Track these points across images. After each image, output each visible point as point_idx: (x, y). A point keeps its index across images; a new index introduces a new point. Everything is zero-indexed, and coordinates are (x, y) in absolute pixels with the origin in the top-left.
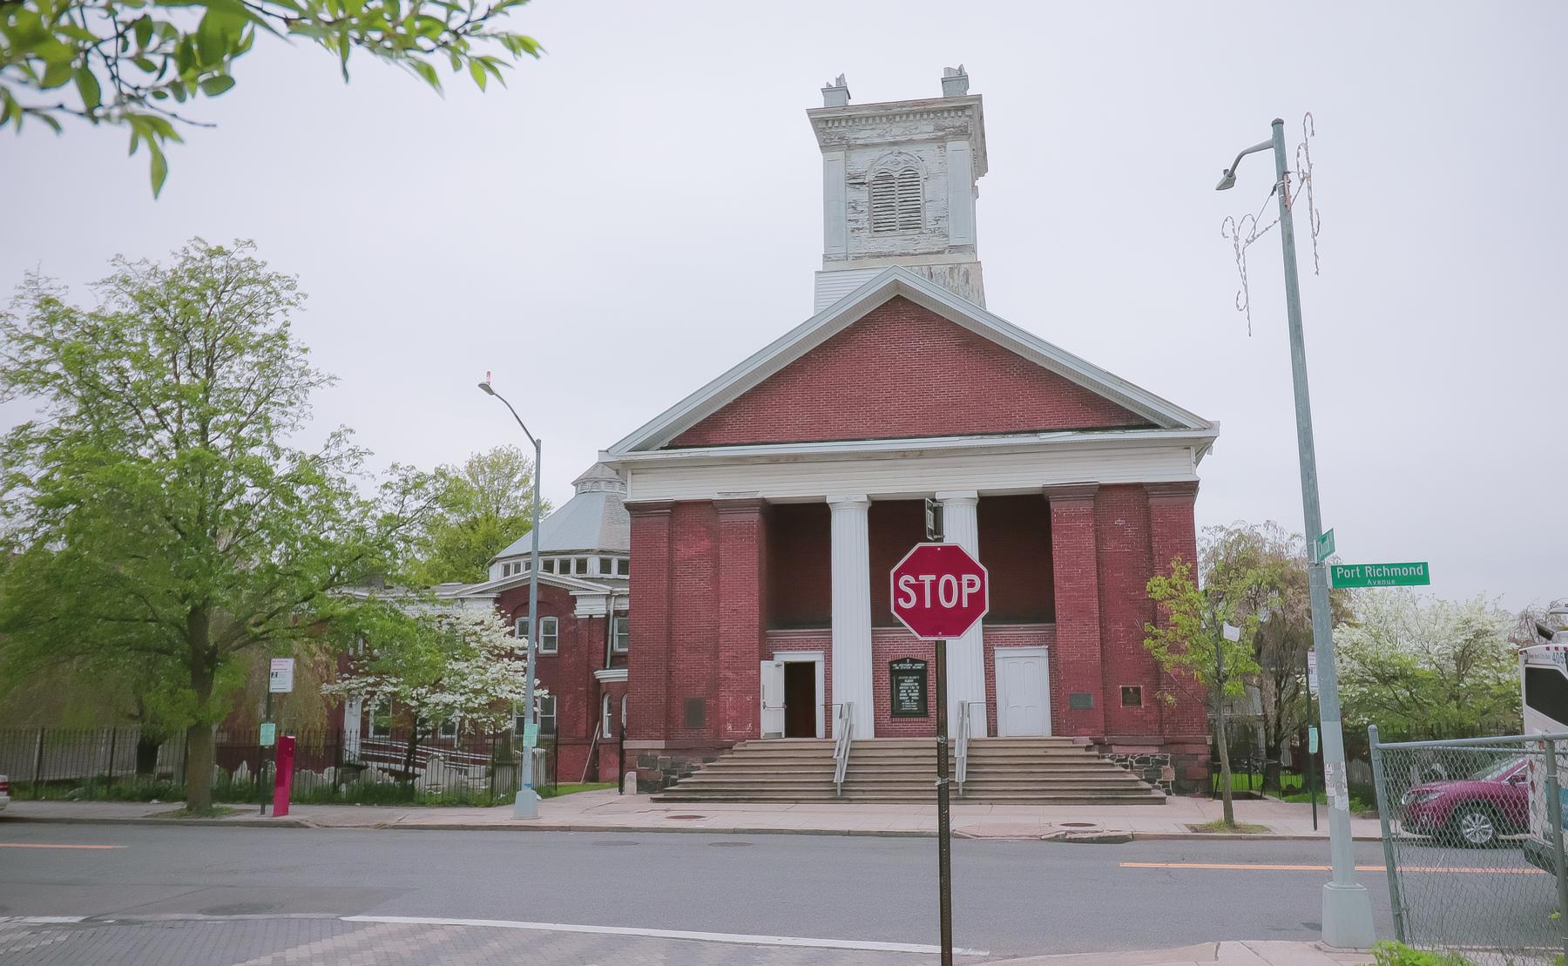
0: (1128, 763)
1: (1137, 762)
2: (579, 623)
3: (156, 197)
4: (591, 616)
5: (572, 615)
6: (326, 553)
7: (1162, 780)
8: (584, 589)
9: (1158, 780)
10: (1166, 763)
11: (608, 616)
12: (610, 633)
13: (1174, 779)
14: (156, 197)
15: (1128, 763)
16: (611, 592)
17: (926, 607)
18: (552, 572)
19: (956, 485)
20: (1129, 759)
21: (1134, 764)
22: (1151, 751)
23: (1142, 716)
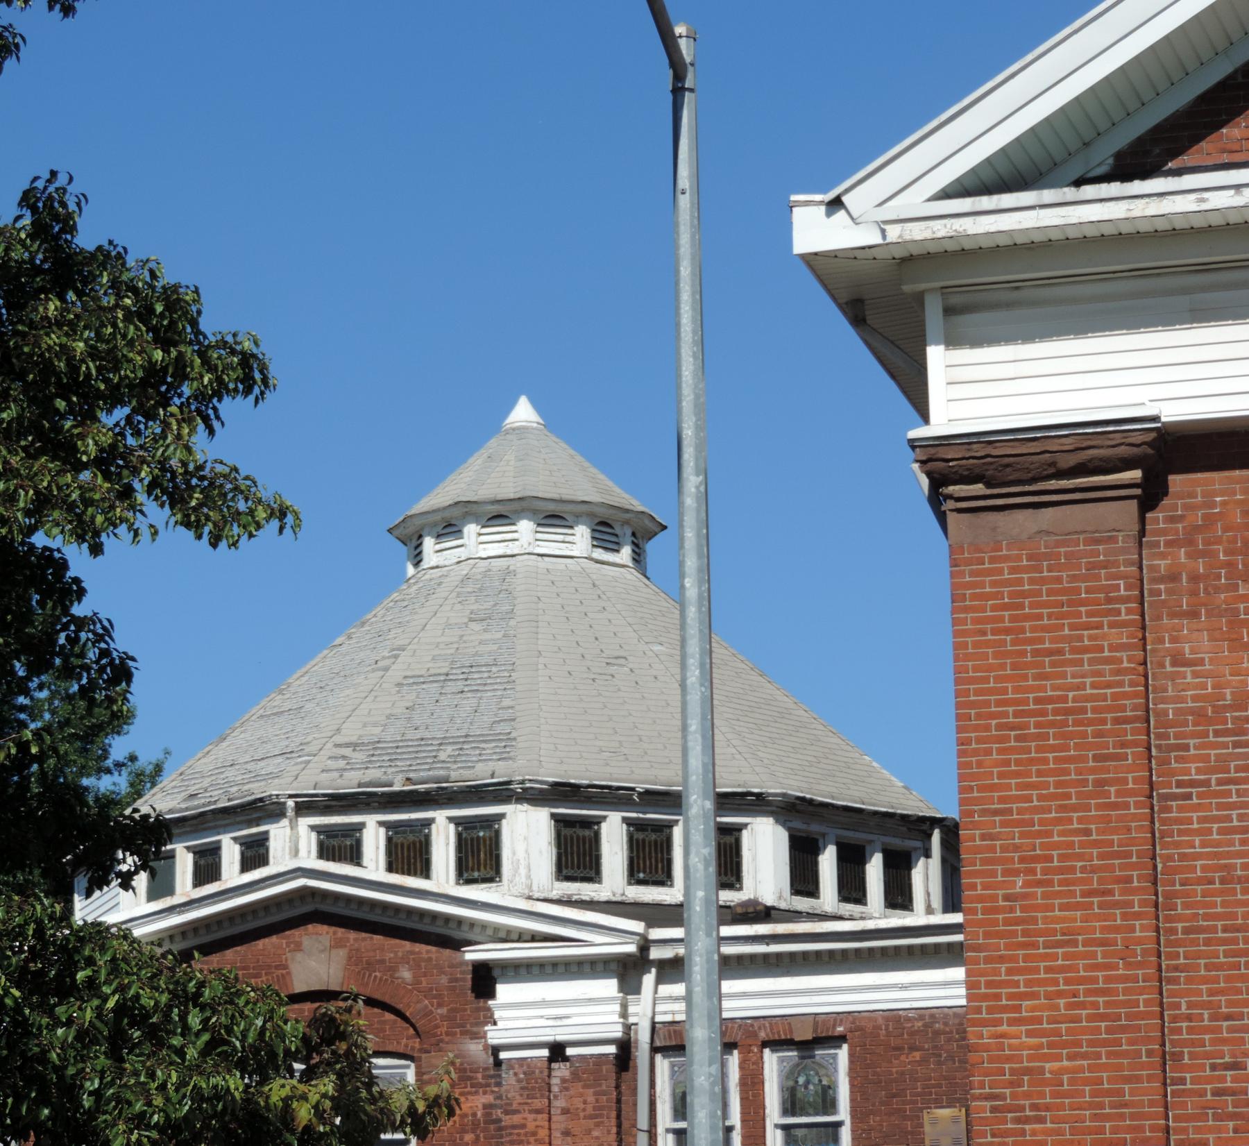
2: (508, 1078)
3: (929, 200)
4: (557, 1051)
5: (474, 1049)
6: (481, 834)
8: (535, 937)
11: (625, 1047)
12: (643, 1123)
14: (929, 200)
16: (645, 945)
17: (957, 997)
18: (424, 870)
19: (1010, 370)
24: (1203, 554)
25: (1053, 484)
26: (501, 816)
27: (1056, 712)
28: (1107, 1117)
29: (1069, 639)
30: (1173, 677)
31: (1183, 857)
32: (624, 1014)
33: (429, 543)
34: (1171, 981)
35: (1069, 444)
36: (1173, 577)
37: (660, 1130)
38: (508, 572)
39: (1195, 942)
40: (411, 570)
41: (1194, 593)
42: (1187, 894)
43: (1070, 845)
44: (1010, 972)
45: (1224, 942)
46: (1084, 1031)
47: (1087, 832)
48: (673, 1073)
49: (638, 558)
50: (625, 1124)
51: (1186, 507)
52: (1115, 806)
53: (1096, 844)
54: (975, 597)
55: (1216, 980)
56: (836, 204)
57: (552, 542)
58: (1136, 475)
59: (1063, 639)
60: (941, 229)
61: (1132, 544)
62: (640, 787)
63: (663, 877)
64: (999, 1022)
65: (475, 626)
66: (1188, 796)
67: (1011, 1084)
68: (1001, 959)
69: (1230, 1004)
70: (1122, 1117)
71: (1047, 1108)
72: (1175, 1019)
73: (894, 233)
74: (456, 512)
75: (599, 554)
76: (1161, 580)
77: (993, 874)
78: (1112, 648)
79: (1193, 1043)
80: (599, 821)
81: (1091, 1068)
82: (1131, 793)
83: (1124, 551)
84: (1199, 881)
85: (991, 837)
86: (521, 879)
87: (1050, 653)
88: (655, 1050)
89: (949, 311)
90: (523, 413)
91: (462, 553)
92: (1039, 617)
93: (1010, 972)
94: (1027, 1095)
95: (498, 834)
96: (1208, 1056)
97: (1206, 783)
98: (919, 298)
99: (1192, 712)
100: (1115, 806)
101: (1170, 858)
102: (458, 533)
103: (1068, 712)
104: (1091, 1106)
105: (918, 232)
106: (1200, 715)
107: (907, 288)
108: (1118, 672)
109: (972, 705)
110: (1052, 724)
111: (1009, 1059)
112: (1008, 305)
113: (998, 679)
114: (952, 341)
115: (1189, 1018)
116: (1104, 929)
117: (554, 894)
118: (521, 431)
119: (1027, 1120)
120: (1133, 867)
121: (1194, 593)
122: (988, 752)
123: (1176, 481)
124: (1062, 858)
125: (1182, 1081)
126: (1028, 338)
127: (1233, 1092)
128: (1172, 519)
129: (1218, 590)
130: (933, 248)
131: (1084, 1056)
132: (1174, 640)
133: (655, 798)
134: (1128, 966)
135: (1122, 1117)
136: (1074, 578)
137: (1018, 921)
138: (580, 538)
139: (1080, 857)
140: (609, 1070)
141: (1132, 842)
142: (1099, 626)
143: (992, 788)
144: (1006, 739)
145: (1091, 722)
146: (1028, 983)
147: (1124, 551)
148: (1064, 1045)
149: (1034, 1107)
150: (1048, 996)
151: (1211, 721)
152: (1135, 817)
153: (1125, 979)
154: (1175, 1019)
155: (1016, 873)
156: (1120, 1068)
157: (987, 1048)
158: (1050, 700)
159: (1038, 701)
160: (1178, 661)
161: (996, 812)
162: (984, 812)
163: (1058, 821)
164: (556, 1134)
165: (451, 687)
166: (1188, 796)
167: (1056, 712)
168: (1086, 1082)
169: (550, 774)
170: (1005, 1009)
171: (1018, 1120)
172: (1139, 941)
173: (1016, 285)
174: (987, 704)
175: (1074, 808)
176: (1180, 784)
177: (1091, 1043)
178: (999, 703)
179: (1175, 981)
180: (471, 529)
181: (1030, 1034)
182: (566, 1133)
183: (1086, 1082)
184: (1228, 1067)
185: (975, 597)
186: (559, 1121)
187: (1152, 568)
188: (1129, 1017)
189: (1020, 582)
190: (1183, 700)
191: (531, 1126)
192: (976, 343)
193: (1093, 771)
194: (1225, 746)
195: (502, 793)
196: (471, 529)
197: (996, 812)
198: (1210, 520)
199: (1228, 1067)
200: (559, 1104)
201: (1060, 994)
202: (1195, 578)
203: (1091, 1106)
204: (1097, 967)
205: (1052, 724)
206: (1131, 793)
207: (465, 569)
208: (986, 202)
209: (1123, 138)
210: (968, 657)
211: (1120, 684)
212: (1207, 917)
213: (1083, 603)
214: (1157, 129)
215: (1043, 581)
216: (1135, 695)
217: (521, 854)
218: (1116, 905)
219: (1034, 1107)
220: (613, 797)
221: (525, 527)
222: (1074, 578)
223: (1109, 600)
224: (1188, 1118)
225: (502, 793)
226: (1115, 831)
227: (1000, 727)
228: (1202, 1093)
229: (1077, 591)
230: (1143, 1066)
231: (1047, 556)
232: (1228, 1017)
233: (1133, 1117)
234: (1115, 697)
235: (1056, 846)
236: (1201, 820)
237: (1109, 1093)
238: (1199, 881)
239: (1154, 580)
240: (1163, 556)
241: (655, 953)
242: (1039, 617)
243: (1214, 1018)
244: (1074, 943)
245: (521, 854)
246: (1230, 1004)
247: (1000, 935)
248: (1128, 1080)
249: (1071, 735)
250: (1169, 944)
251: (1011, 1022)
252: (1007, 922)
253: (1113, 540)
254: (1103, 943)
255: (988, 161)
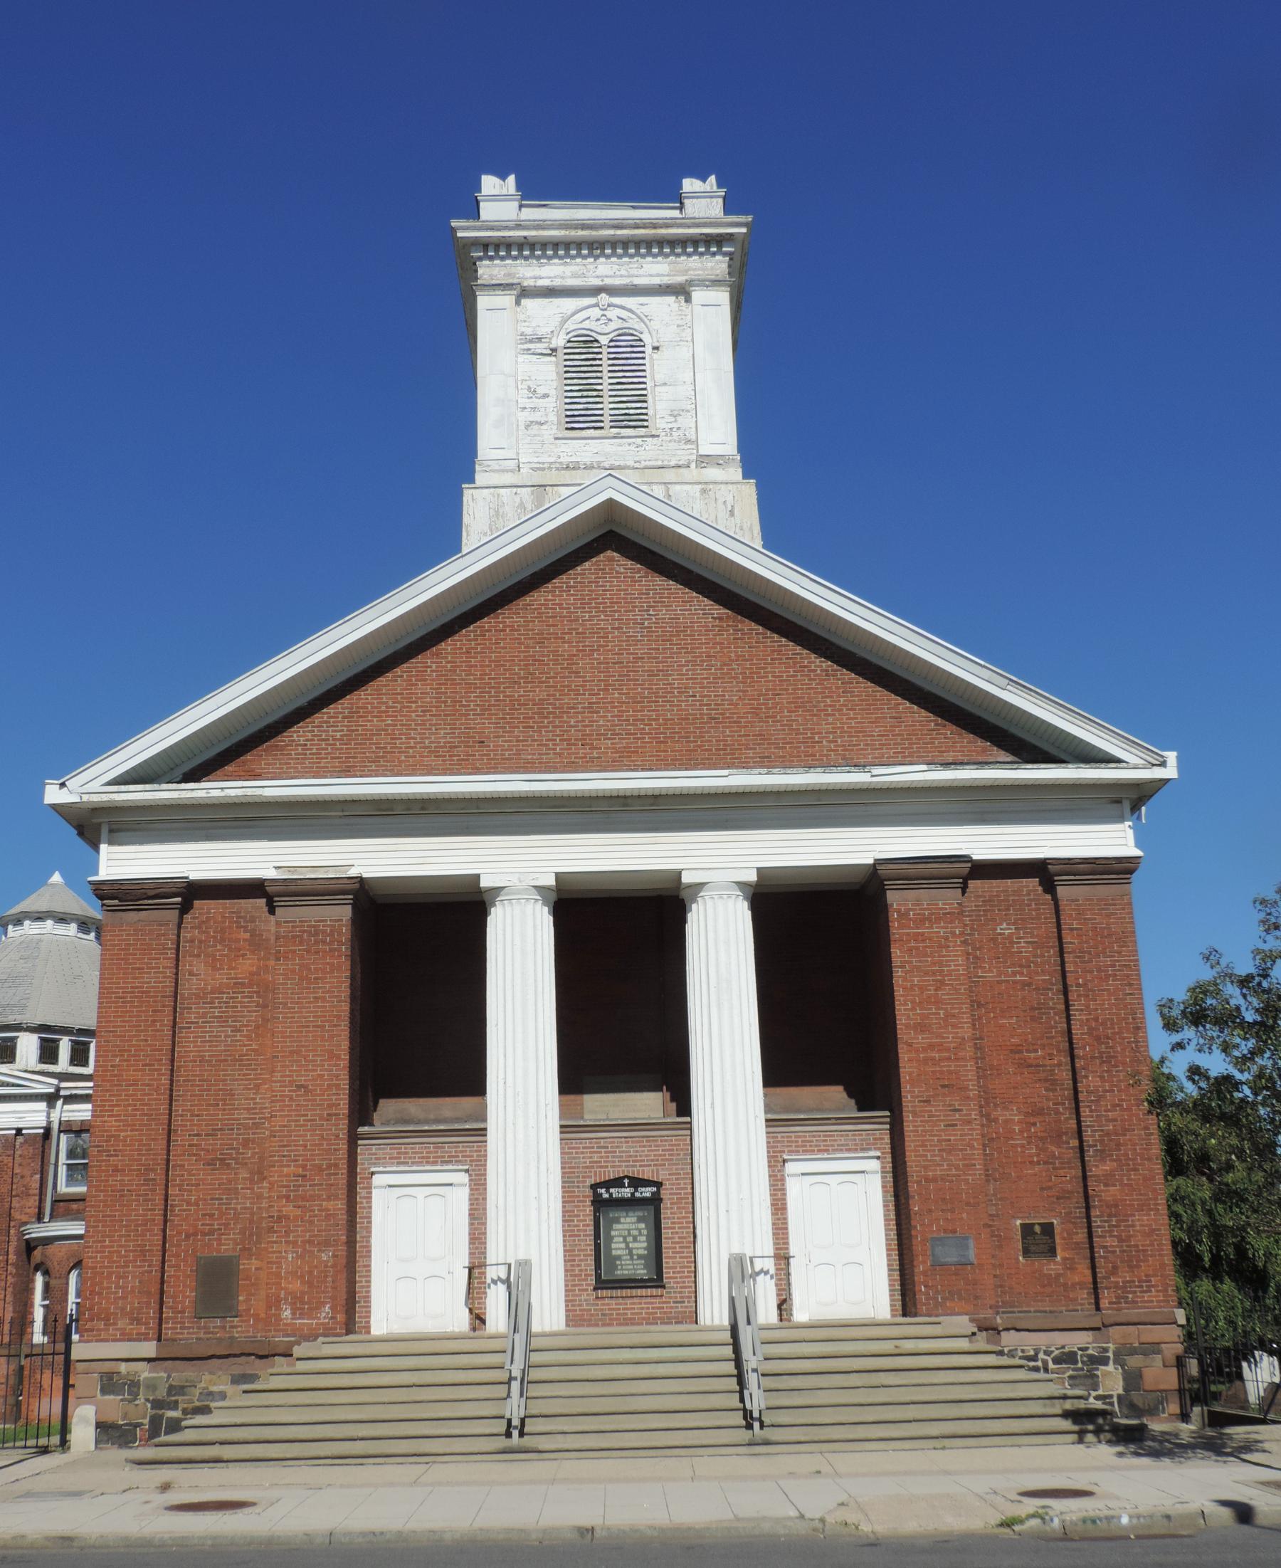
0: (1039, 1364)
1: (1056, 1361)
7: (1100, 1392)
8: (8, 1085)
9: (1094, 1394)
10: (1105, 1361)
11: (48, 1131)
12: (53, 1160)
13: (1121, 1391)
15: (1039, 1364)
16: (58, 1089)
19: (133, 855)
20: (1041, 1356)
21: (1051, 1365)
22: (1075, 1341)
23: (1058, 1276)
24: (204, 932)
25: (146, 902)
26: (18, 1037)
27: (138, 992)
28: (144, 1155)
29: (147, 963)
30: (188, 980)
31: (186, 1051)
32: (48, 1116)
33: (10, 927)
34: (176, 1101)
35: (152, 886)
36: (192, 941)
37: (60, 1164)
38: (40, 940)
39: (187, 1086)
40: (4, 938)
41: (200, 948)
42: (187, 1066)
43: (140, 1046)
44: (110, 1096)
45: (199, 1086)
46: (138, 1120)
47: (146, 1041)
48: (68, 1141)
49: (98, 938)
50: (46, 1161)
51: (200, 914)
52: (158, 1030)
53: (149, 1045)
54: (111, 945)
55: (194, 1100)
56: (63, 785)
57: (61, 929)
58: (179, 899)
59: (145, 963)
60: (105, 798)
61: (175, 927)
62: (77, 1027)
63: (84, 1063)
64: (104, 1116)
65: (22, 961)
66: (190, 1028)
67: (106, 1141)
68: (107, 1091)
69: (199, 1110)
70: (149, 1155)
71: (120, 1151)
72: (176, 1116)
73: (85, 798)
74: (21, 915)
75: (80, 935)
76: (187, 942)
77: (107, 1056)
78: (164, 968)
79: (182, 1126)
80: (59, 1040)
81: (140, 1135)
82: (165, 1025)
83: (172, 929)
84: (191, 1061)
85: (108, 1042)
86: (24, 1062)
87: (139, 969)
88: (60, 1131)
89: (111, 831)
90: (57, 878)
91: (22, 932)
92: (136, 954)
93: (110, 1096)
94: (112, 1145)
95: (16, 1044)
96: (187, 1131)
97: (197, 1023)
98: (100, 824)
99: (194, 994)
100: (158, 1030)
101: (180, 1052)
102: (22, 924)
103: (143, 992)
104: (138, 1150)
105: (95, 798)
106: (197, 996)
107: (95, 821)
108: (164, 977)
109: (106, 988)
110: (136, 997)
111: (106, 1131)
112: (135, 830)
113: (117, 978)
114: (111, 843)
115: (182, 1116)
116: (150, 1080)
117: (37, 1069)
118: (53, 885)
119: (112, 1156)
120: (163, 1055)
121: (200, 948)
122: (110, 1007)
123: (197, 903)
124: (136, 1051)
125: (177, 1141)
126: (141, 843)
127: (196, 1145)
128: (194, 918)
129: (209, 946)
130: (101, 805)
131: (136, 1130)
132: (190, 965)
133: (82, 1032)
134: (158, 1094)
135: (149, 1155)
136: (150, 939)
137: (115, 1076)
138: (73, 928)
139: (142, 1050)
140: (40, 1140)
141: (163, 1045)
142: (159, 959)
143: (110, 1022)
144: (118, 1002)
145: (152, 997)
146: (117, 1101)
147: (172, 929)
148: (129, 1126)
149: (115, 1150)
150: (125, 1106)
151: (201, 998)
152: (166, 1035)
153: (156, 1099)
154: (176, 1116)
155: (117, 1056)
156: (150, 1135)
157: (98, 1126)
158: (137, 987)
159: (132, 987)
160: (191, 974)
161: (111, 1032)
162: (106, 1032)
163: (135, 1036)
164: (16, 1165)
165: (6, 985)
166: (190, 1028)
167: (138, 992)
168: (137, 1140)
169: (39, 1021)
170: (107, 1111)
171: (107, 1156)
172: (163, 1085)
173: (139, 822)
174: (111, 988)
175: (142, 1031)
176: (187, 1023)
177: (140, 1125)
178: (117, 988)
179: (178, 1101)
180: (27, 923)
181: (116, 1121)
182: (20, 1165)
183: (137, 1140)
184: (195, 1135)
185: (111, 945)
186: (18, 1160)
187: (184, 937)
188: (156, 1115)
189: (129, 940)
190: (191, 989)
191: (5, 1161)
192: (121, 844)
193: (151, 1016)
194: (206, 1008)
195: (18, 1028)
196: (27, 923)
197: (111, 1032)
198: (208, 919)
199: (195, 1135)
200: (18, 1153)
201: (129, 1105)
202: (200, 942)
203: (138, 1150)
204: (145, 1095)
205: (136, 997)
206: (165, 1025)
207: (22, 938)
208: (123, 788)
209: (187, 767)
210: (106, 969)
211: (165, 982)
212: (193, 1076)
213: (154, 949)
214: (200, 765)
215: (138, 940)
216: (171, 987)
217: (24, 1053)
218: (156, 1070)
219: (115, 1150)
220: (65, 1031)
221: (49, 923)
222: (150, 939)
223: (164, 949)
224: (179, 1156)
225: (18, 1028)
226: (157, 1040)
227: (116, 997)
228: (184, 1145)
229: (151, 944)
230: (160, 1134)
231: (141, 930)
232: (198, 1116)
233: (154, 1155)
234: (163, 987)
235: (133, 1046)
236: (194, 1037)
237: (145, 1145)
238: (191, 1061)
239: (184, 942)
240: (189, 932)
241: (62, 1093)
242: (136, 954)
243: (192, 1115)
244: (137, 1085)
245: (24, 1053)
246: (199, 1110)
247: (108, 1081)
248: (154, 1140)
249: (143, 1002)
250: (177, 1086)
251: (109, 1116)
252: (111, 1076)
253: (168, 925)
254: (148, 1085)
255: (127, 772)
